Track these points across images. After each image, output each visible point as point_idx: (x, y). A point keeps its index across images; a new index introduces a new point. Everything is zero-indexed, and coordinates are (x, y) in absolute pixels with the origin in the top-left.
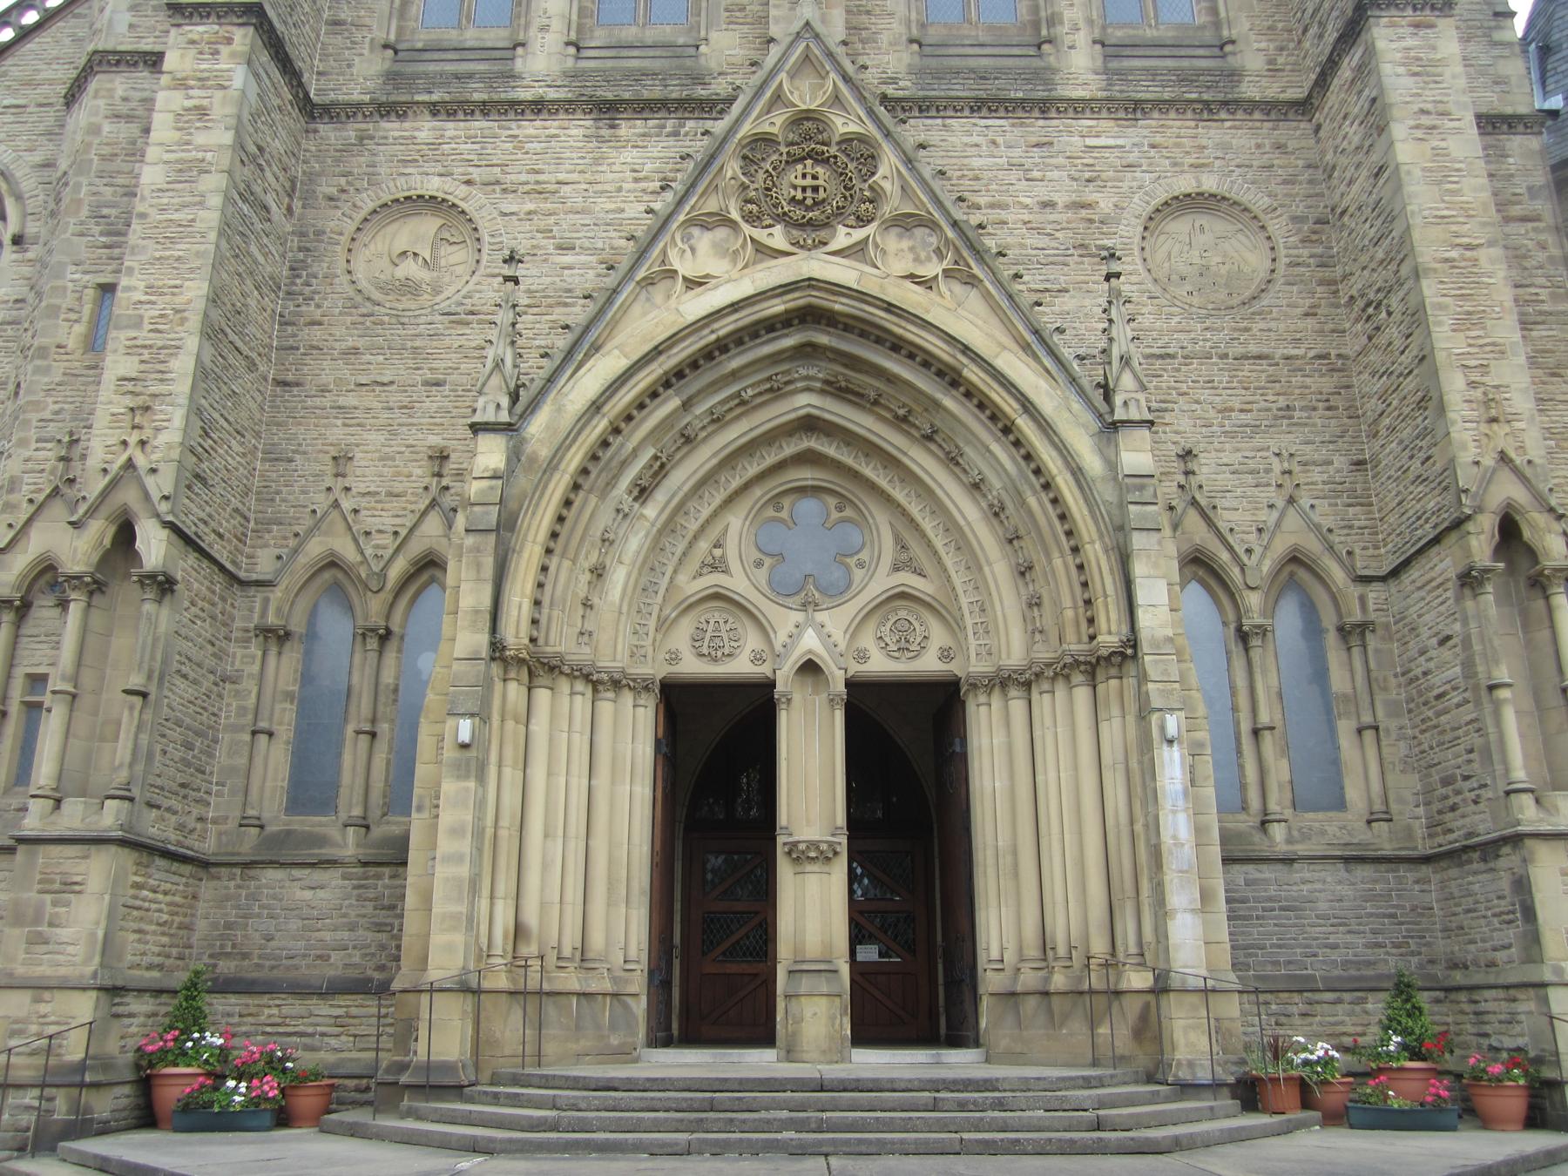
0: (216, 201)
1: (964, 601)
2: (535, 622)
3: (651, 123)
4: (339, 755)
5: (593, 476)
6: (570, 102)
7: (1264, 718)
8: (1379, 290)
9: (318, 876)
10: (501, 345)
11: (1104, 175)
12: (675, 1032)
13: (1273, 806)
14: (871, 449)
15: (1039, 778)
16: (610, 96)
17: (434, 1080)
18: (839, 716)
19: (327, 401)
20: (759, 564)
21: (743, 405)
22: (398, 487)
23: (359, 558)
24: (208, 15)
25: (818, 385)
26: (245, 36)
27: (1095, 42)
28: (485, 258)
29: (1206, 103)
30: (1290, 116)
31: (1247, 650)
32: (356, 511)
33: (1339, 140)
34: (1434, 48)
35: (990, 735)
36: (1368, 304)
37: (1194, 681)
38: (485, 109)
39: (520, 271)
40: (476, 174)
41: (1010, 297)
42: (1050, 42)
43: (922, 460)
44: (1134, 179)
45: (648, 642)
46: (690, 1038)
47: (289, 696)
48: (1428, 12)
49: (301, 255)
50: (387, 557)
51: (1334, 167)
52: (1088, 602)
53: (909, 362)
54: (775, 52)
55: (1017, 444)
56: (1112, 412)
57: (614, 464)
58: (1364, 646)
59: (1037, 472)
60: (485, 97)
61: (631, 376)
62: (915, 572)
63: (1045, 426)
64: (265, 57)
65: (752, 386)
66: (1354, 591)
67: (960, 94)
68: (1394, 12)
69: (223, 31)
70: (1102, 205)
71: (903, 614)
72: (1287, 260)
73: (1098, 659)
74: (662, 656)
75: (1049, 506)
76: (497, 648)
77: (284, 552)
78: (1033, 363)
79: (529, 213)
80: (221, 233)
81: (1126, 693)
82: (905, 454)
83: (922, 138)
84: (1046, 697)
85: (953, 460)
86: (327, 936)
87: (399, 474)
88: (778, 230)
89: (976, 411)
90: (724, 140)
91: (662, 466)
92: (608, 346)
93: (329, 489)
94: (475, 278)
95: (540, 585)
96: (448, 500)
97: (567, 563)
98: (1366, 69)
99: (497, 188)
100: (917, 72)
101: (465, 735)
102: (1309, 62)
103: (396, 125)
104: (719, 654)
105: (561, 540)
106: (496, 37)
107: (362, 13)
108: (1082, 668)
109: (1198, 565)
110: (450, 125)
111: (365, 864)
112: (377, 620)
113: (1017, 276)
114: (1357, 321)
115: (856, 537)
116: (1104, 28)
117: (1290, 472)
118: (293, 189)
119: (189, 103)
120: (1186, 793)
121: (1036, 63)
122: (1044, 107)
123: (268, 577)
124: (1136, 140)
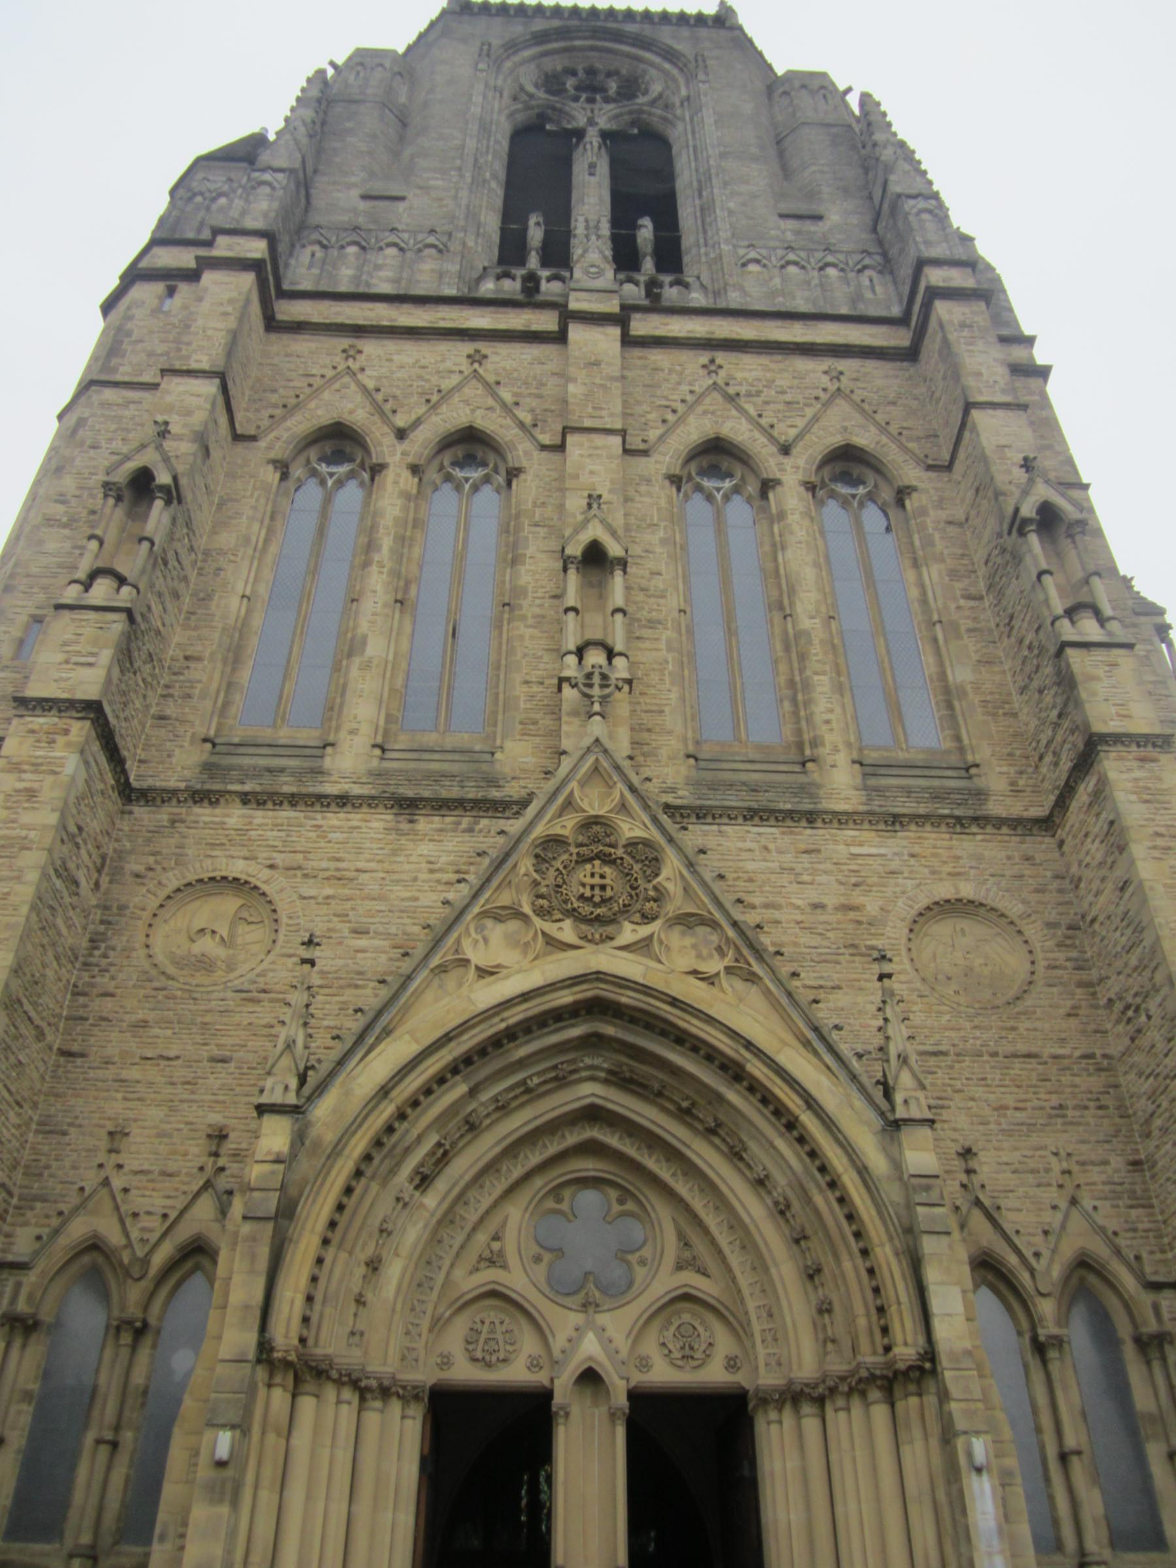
0: (33, 876)
1: (751, 1305)
2: (306, 1320)
3: (448, 819)
4: (72, 1469)
5: (376, 1162)
6: (373, 798)
7: (1071, 1442)
8: (1136, 995)
10: (294, 1024)
11: (869, 881)
15: (839, 1510)
16: (410, 793)
18: (621, 1432)
19: (110, 1073)
20: (538, 1259)
21: (528, 1093)
22: (172, 1166)
23: (124, 1241)
24: (50, 709)
25: (603, 1075)
26: (81, 729)
27: (854, 762)
28: (281, 937)
29: (958, 819)
30: (1035, 831)
31: (1044, 1362)
32: (126, 1190)
33: (1082, 855)
34: (1160, 779)
35: (784, 1456)
36: (1128, 1007)
37: (996, 1397)
38: (293, 800)
39: (316, 953)
40: (279, 859)
41: (789, 994)
42: (813, 761)
43: (704, 1154)
44: (897, 885)
45: (420, 1345)
47: (27, 1396)
48: (1150, 748)
49: (102, 928)
50: (153, 1240)
51: (1080, 879)
52: (881, 1310)
53: (693, 1055)
54: (566, 764)
55: (801, 1140)
56: (893, 1110)
57: (399, 1150)
59: (823, 1169)
60: (294, 789)
61: (421, 1062)
62: (698, 1271)
63: (829, 1123)
64: (96, 747)
65: (538, 1074)
66: (1145, 1299)
67: (733, 804)
68: (1120, 748)
69: (61, 723)
70: (869, 908)
72: (1045, 963)
73: (896, 1373)
74: (434, 1359)
75: (835, 1205)
76: (264, 1347)
77: (45, 1232)
78: (814, 1060)
79: (328, 897)
80: (33, 907)
81: (927, 1413)
82: (689, 1147)
83: (700, 842)
84: (842, 1415)
85: (736, 1155)
87: (174, 1152)
88: (568, 924)
89: (760, 1105)
90: (519, 840)
91: (446, 1153)
93: (101, 1166)
94: (270, 957)
95: (314, 1279)
96: (223, 1182)
97: (343, 1256)
98: (1100, 794)
99: (299, 873)
101: (223, 1450)
102: (1047, 785)
103: (208, 811)
104: (494, 1358)
106: (308, 736)
107: (187, 710)
108: (879, 1382)
109: (989, 1270)
110: (259, 813)
112: (133, 1311)
113: (795, 975)
114: (1118, 1022)
115: (637, 1231)
116: (861, 750)
117: (1069, 1172)
118: (103, 864)
120: (1000, 1531)
121: (801, 779)
122: (811, 818)
123: (25, 1259)
124: (896, 850)
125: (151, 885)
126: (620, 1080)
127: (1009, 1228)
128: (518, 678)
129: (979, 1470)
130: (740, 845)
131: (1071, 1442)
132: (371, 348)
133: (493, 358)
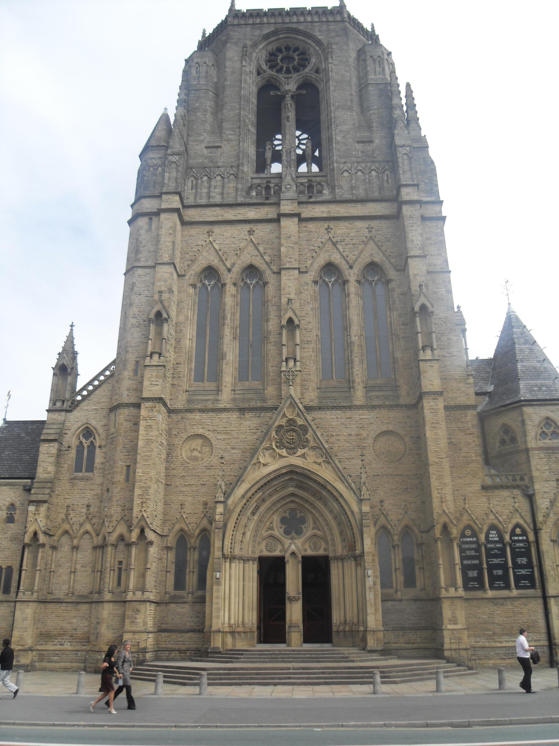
9: (183, 605)
12: (262, 640)
13: (399, 588)
14: (306, 501)
17: (215, 651)
19: (178, 489)
21: (276, 491)
28: (214, 451)
31: (394, 549)
38: (213, 410)
40: (210, 428)
43: (319, 504)
46: (265, 642)
47: (173, 562)
58: (422, 548)
71: (315, 540)
85: (326, 505)
86: (186, 619)
88: (284, 450)
92: (246, 480)
94: (212, 457)
100: (319, 398)
103: (190, 415)
105: (236, 528)
111: (194, 603)
119: (148, 424)
122: (350, 408)
125: (180, 437)
126: (297, 487)
127: (389, 519)
128: (270, 365)
129: (369, 577)
130: (331, 417)
131: (397, 566)
132: (217, 230)
133: (257, 231)
